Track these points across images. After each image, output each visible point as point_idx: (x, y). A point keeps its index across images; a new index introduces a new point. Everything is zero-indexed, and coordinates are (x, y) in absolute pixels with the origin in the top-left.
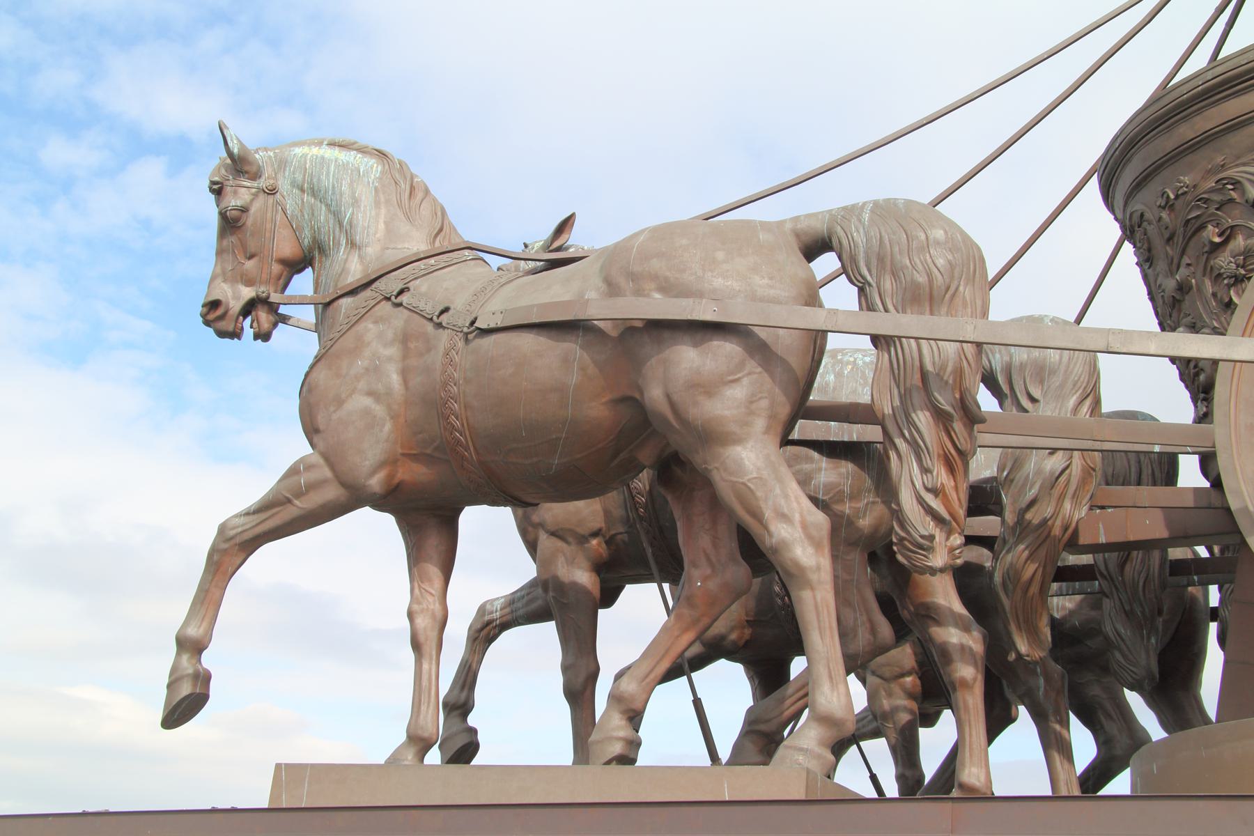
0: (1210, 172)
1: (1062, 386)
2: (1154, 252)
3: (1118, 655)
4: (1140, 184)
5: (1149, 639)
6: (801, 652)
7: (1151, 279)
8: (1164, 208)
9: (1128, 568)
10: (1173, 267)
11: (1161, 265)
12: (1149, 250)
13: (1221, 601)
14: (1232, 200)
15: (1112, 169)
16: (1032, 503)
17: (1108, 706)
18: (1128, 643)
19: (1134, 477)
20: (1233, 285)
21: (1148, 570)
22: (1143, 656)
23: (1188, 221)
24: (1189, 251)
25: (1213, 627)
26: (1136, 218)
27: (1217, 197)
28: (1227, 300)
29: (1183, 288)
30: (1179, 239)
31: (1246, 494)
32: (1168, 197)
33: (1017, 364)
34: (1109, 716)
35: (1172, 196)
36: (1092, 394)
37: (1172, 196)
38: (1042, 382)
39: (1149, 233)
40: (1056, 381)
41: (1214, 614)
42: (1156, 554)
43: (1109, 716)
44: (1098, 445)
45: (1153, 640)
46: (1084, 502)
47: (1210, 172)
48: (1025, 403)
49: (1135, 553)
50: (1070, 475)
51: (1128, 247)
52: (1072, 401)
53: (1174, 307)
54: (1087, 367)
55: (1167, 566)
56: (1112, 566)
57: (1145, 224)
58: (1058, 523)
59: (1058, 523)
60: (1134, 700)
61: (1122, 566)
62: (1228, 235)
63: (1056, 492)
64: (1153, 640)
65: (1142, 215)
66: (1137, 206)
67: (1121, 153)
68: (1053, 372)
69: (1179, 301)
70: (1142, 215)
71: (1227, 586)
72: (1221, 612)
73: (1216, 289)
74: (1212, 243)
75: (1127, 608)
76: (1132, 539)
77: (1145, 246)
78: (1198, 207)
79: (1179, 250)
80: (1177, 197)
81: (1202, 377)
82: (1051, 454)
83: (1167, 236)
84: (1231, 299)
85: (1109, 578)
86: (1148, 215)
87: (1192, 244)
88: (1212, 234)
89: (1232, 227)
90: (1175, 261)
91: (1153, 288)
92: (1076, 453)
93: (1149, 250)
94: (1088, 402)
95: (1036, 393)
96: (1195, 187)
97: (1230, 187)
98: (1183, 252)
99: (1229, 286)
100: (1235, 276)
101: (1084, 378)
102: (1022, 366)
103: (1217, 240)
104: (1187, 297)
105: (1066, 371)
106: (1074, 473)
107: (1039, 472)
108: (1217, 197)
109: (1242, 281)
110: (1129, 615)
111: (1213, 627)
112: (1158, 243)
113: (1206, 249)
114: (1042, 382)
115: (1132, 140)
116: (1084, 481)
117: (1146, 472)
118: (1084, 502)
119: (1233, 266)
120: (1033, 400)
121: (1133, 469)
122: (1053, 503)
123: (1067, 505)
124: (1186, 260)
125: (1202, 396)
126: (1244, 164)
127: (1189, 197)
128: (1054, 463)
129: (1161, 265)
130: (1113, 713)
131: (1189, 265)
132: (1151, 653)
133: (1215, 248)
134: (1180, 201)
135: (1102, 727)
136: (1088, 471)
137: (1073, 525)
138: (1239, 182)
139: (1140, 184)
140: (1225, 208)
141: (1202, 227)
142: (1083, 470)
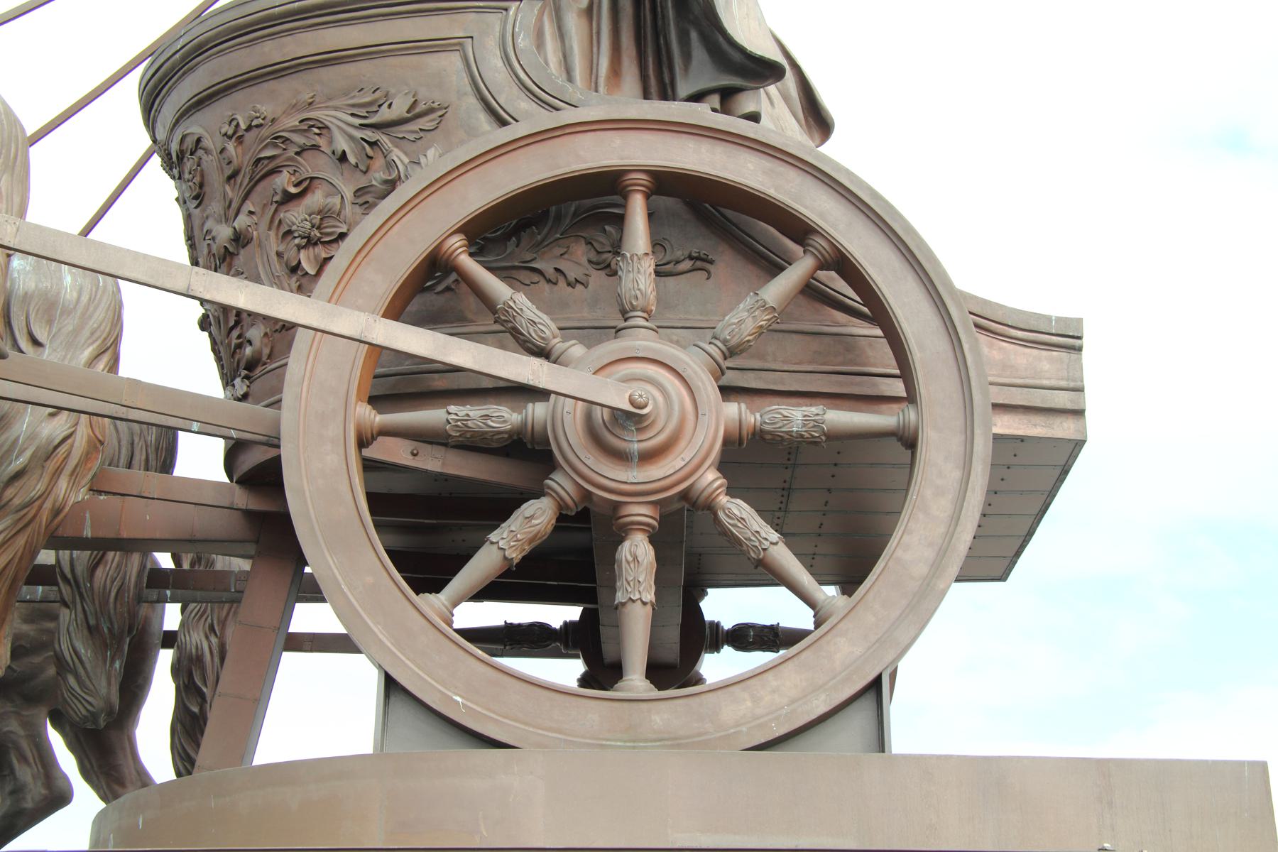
0: (295, 107)
1: (77, 332)
2: (206, 189)
3: (72, 680)
4: (200, 103)
5: (113, 661)
6: (307, 564)
7: (197, 223)
8: (230, 138)
9: (99, 572)
10: (230, 212)
11: (215, 207)
12: (201, 185)
13: (182, 624)
14: (315, 147)
15: (165, 75)
16: (18, 475)
17: (25, 744)
18: (88, 666)
19: (123, 460)
20: (304, 247)
21: (125, 573)
22: (104, 683)
23: (260, 160)
24: (255, 196)
25: (165, 658)
26: (190, 143)
27: (299, 139)
28: (294, 263)
29: (240, 239)
30: (244, 179)
31: (307, 494)
32: (238, 125)
33: (21, 292)
34: (23, 759)
35: (243, 126)
36: (110, 349)
37: (243, 126)
38: (50, 322)
39: (204, 164)
40: (69, 325)
41: (169, 639)
42: (136, 558)
43: (23, 759)
44: (122, 412)
45: (117, 665)
46: (83, 482)
47: (295, 107)
48: (24, 343)
49: (111, 554)
50: (72, 446)
51: (156, 175)
52: (87, 353)
53: (224, 260)
54: (110, 313)
55: (146, 574)
56: (80, 569)
57: (200, 153)
58: (48, 505)
59: (48, 505)
60: (56, 740)
61: (93, 569)
62: (307, 186)
63: (51, 465)
64: (117, 665)
65: (199, 140)
66: (194, 127)
67: (183, 58)
68: (67, 312)
69: (232, 254)
70: (199, 140)
71: (192, 606)
72: (181, 637)
73: (281, 248)
74: (285, 192)
75: (92, 622)
76: (125, 535)
77: (197, 180)
78: (275, 146)
79: (242, 193)
80: (249, 128)
81: (248, 350)
82: (52, 415)
83: (228, 172)
84: (299, 262)
85: (74, 583)
86: (207, 142)
87: (259, 188)
88: (284, 181)
89: (312, 179)
90: (235, 205)
91: (197, 232)
92: (580, 403)
93: (201, 185)
94: (105, 358)
95: (41, 335)
96: (273, 120)
97: (317, 131)
98: (246, 197)
99: (299, 248)
100: (308, 238)
101: (106, 327)
102: (27, 298)
103: (293, 190)
104: (242, 252)
105: (83, 314)
106: (77, 444)
107: (32, 437)
108: (299, 139)
109: (316, 244)
110: (92, 631)
111: (165, 658)
112: (215, 179)
113: (277, 198)
114: (50, 322)
115: (200, 46)
116: (87, 457)
117: (139, 457)
118: (83, 482)
119: (308, 225)
120: (36, 343)
121: (124, 452)
122: (46, 479)
123: (63, 484)
124: (249, 206)
125: (244, 373)
126: (336, 108)
127: (265, 132)
128: (56, 427)
129: (215, 207)
130: (31, 760)
131: (251, 213)
132: (113, 680)
133: (288, 198)
134: (254, 132)
135: (12, 771)
136: (96, 444)
137: (67, 509)
138: (327, 127)
139: (200, 103)
140: (305, 154)
141: (275, 171)
142: (89, 441)
